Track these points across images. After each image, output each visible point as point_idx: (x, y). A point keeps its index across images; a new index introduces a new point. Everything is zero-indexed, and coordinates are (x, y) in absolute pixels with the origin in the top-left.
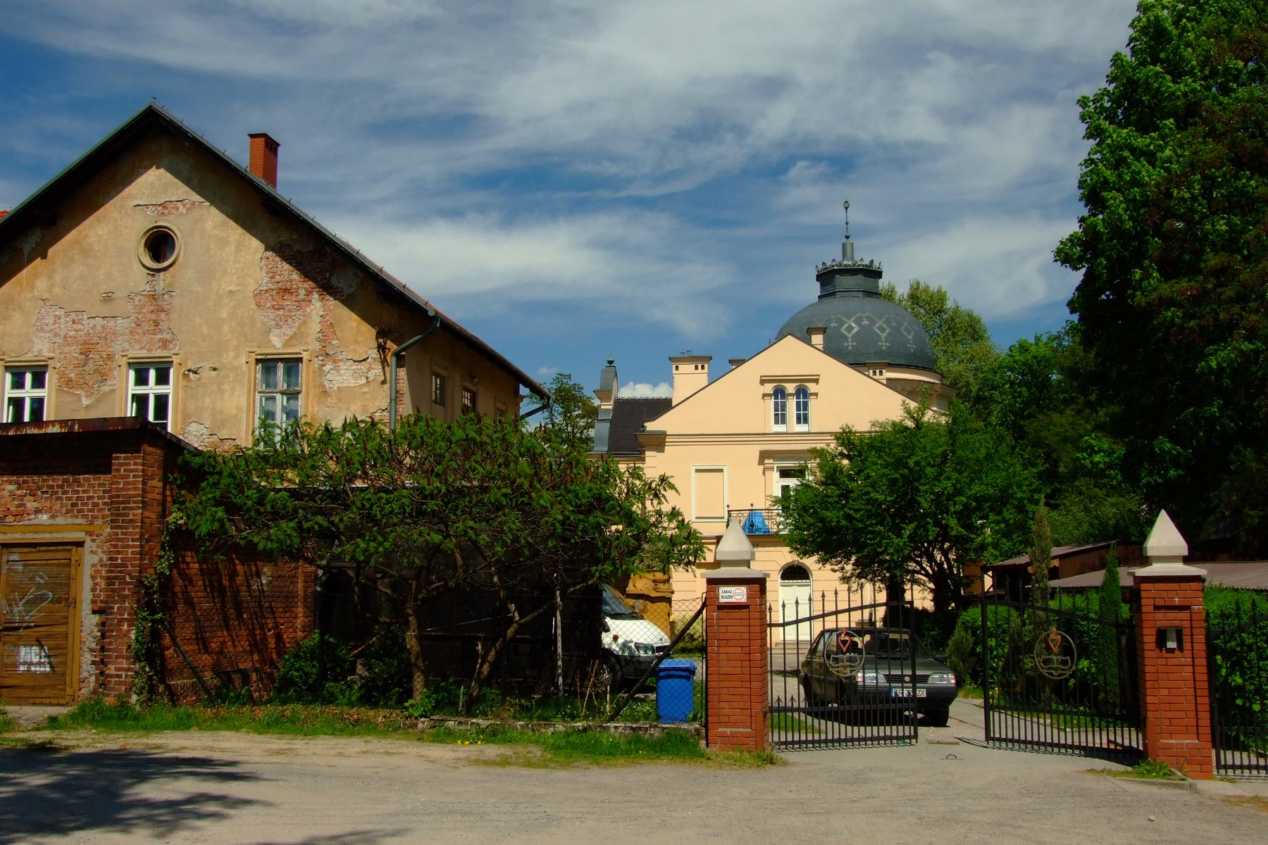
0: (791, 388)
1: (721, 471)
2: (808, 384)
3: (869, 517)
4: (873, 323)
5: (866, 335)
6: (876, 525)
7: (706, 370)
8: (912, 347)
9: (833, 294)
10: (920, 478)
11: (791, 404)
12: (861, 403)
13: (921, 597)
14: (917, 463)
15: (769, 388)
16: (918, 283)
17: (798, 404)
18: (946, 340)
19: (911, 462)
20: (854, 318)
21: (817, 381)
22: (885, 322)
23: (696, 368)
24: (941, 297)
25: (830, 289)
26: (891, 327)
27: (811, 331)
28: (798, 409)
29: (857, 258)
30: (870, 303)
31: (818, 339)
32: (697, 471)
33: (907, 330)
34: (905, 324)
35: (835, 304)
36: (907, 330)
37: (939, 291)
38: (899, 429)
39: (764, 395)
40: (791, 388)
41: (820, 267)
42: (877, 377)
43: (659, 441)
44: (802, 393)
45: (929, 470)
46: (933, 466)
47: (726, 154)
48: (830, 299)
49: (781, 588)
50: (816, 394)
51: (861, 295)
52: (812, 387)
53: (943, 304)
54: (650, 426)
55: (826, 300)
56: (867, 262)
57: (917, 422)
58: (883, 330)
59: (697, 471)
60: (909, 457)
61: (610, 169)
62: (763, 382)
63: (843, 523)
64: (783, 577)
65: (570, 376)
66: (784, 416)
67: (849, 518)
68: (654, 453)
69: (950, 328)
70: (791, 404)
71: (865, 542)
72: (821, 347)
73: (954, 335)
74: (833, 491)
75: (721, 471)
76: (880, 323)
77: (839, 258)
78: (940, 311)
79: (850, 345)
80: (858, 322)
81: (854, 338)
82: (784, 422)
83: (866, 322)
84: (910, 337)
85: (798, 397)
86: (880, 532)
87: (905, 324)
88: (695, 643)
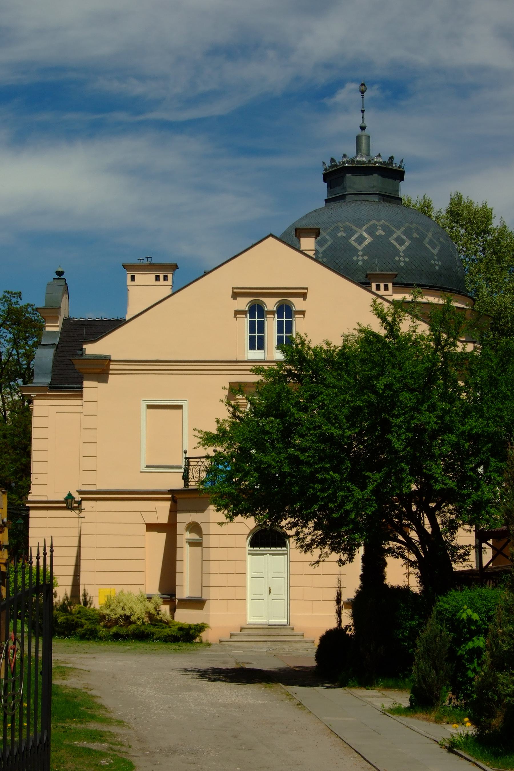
0: (271, 304)
1: (180, 407)
2: (293, 300)
3: (321, 459)
4: (389, 232)
5: (380, 248)
6: (326, 470)
7: (169, 282)
8: (437, 264)
9: (342, 198)
10: (393, 406)
11: (271, 325)
12: (337, 313)
13: (399, 573)
14: (388, 386)
15: (243, 303)
16: (460, 197)
17: (280, 324)
18: (489, 265)
19: (380, 384)
20: (365, 227)
21: (304, 296)
22: (405, 233)
23: (157, 278)
24: (486, 216)
25: (338, 191)
26: (411, 239)
27: (300, 232)
28: (280, 330)
29: (374, 154)
30: (387, 210)
31: (308, 243)
32: (149, 407)
33: (431, 243)
34: (430, 235)
35: (345, 210)
36: (431, 243)
37: (484, 207)
38: (369, 338)
39: (237, 312)
40: (271, 304)
41: (328, 164)
42: (382, 292)
43: (101, 369)
44: (285, 310)
45: (405, 395)
46: (412, 391)
47: (268, 75)
48: (339, 203)
49: (249, 558)
50: (303, 313)
51: (376, 199)
52: (298, 304)
53: (488, 224)
54: (91, 349)
55: (334, 205)
56: (385, 159)
57: (392, 328)
58: (401, 242)
59: (149, 407)
60: (377, 377)
61: (137, 89)
62: (235, 295)
63: (286, 469)
64: (253, 544)
65: (19, 294)
66: (261, 340)
67: (294, 461)
68: (94, 384)
69: (495, 253)
70: (271, 325)
71: (314, 495)
72: (311, 254)
73: (499, 261)
74: (271, 424)
75: (180, 407)
76: (398, 233)
77: (351, 151)
78: (485, 232)
79: (360, 259)
80: (371, 231)
81: (367, 250)
82: (261, 347)
83: (380, 232)
84: (435, 252)
85: (280, 316)
86: (333, 481)
87: (430, 235)
88: (132, 627)
